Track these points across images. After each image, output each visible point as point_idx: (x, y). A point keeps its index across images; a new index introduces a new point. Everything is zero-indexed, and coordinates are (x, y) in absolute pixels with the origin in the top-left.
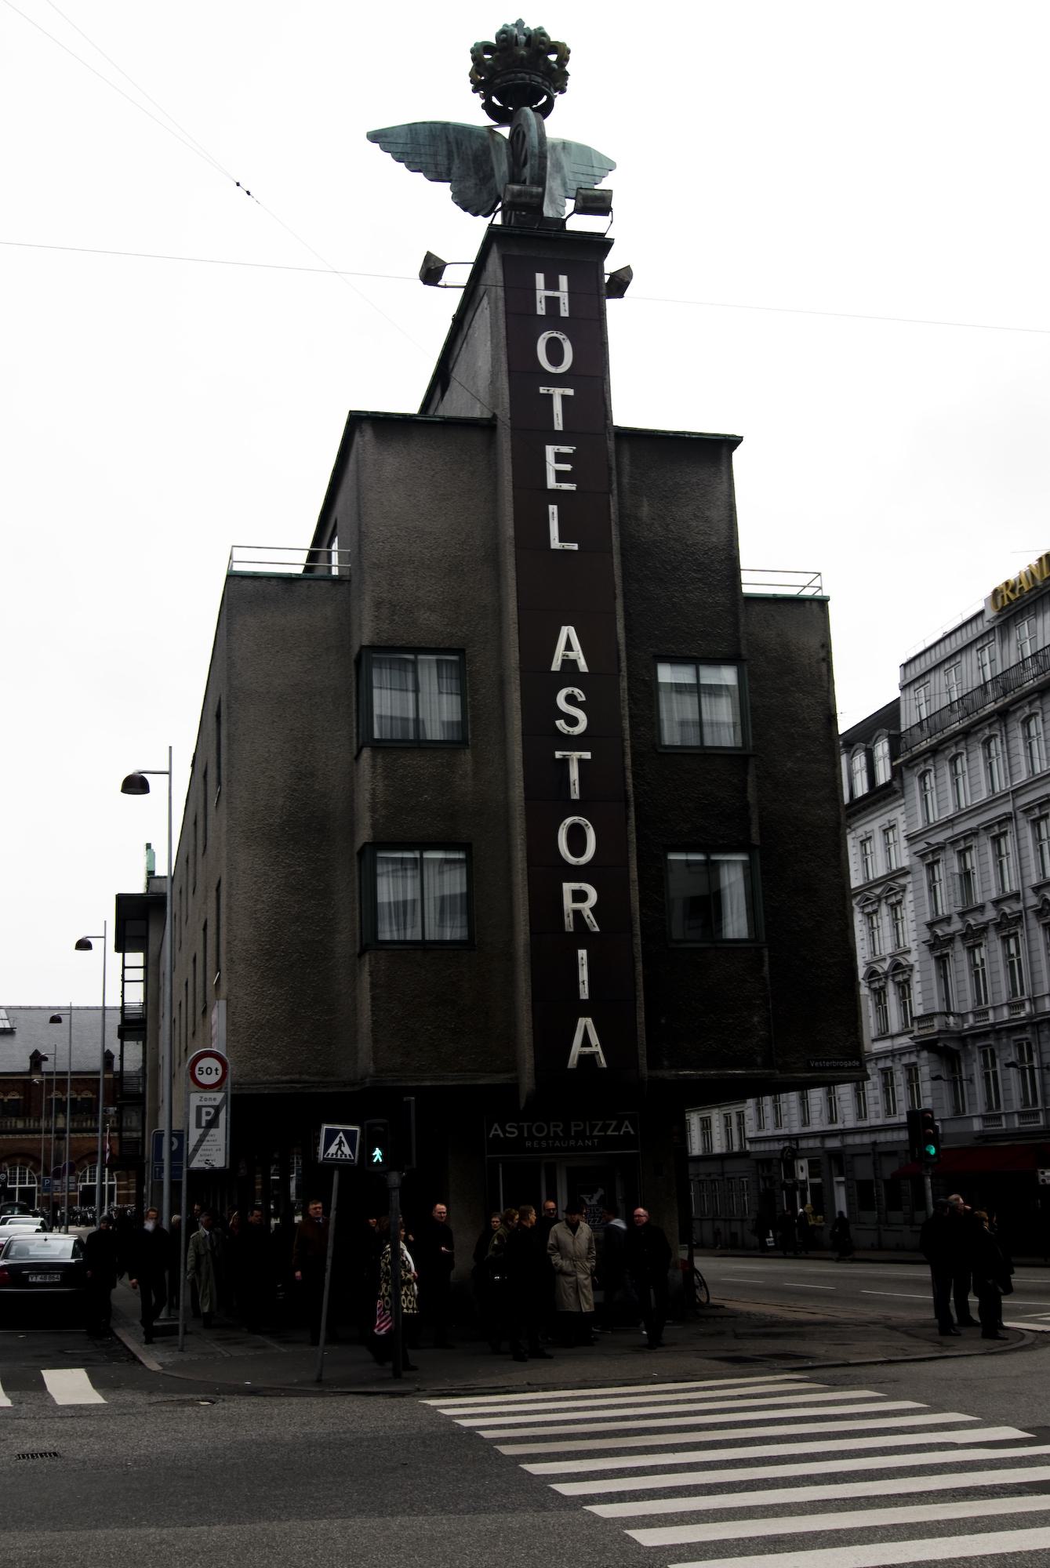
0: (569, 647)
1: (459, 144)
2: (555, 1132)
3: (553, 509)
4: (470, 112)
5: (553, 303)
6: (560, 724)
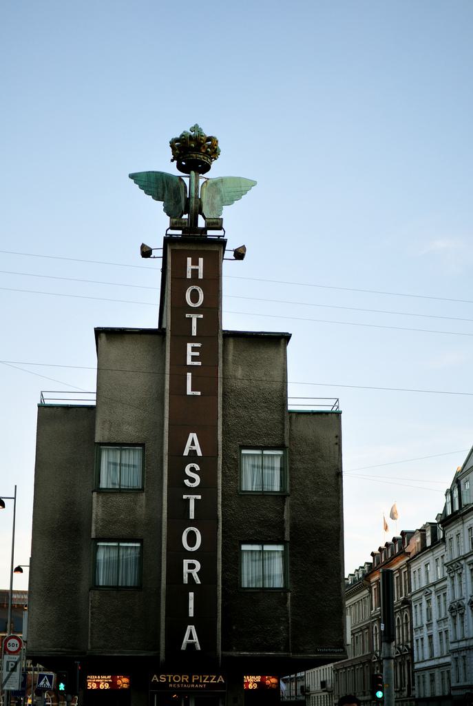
0: (193, 444)
1: (168, 184)
2: (184, 680)
3: (189, 375)
4: (172, 169)
5: (195, 272)
6: (187, 482)
